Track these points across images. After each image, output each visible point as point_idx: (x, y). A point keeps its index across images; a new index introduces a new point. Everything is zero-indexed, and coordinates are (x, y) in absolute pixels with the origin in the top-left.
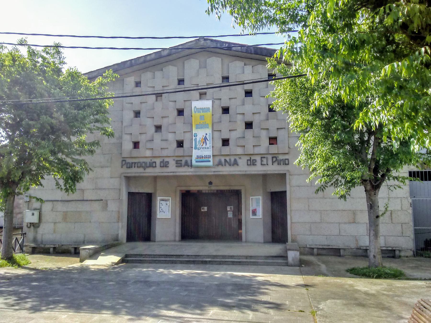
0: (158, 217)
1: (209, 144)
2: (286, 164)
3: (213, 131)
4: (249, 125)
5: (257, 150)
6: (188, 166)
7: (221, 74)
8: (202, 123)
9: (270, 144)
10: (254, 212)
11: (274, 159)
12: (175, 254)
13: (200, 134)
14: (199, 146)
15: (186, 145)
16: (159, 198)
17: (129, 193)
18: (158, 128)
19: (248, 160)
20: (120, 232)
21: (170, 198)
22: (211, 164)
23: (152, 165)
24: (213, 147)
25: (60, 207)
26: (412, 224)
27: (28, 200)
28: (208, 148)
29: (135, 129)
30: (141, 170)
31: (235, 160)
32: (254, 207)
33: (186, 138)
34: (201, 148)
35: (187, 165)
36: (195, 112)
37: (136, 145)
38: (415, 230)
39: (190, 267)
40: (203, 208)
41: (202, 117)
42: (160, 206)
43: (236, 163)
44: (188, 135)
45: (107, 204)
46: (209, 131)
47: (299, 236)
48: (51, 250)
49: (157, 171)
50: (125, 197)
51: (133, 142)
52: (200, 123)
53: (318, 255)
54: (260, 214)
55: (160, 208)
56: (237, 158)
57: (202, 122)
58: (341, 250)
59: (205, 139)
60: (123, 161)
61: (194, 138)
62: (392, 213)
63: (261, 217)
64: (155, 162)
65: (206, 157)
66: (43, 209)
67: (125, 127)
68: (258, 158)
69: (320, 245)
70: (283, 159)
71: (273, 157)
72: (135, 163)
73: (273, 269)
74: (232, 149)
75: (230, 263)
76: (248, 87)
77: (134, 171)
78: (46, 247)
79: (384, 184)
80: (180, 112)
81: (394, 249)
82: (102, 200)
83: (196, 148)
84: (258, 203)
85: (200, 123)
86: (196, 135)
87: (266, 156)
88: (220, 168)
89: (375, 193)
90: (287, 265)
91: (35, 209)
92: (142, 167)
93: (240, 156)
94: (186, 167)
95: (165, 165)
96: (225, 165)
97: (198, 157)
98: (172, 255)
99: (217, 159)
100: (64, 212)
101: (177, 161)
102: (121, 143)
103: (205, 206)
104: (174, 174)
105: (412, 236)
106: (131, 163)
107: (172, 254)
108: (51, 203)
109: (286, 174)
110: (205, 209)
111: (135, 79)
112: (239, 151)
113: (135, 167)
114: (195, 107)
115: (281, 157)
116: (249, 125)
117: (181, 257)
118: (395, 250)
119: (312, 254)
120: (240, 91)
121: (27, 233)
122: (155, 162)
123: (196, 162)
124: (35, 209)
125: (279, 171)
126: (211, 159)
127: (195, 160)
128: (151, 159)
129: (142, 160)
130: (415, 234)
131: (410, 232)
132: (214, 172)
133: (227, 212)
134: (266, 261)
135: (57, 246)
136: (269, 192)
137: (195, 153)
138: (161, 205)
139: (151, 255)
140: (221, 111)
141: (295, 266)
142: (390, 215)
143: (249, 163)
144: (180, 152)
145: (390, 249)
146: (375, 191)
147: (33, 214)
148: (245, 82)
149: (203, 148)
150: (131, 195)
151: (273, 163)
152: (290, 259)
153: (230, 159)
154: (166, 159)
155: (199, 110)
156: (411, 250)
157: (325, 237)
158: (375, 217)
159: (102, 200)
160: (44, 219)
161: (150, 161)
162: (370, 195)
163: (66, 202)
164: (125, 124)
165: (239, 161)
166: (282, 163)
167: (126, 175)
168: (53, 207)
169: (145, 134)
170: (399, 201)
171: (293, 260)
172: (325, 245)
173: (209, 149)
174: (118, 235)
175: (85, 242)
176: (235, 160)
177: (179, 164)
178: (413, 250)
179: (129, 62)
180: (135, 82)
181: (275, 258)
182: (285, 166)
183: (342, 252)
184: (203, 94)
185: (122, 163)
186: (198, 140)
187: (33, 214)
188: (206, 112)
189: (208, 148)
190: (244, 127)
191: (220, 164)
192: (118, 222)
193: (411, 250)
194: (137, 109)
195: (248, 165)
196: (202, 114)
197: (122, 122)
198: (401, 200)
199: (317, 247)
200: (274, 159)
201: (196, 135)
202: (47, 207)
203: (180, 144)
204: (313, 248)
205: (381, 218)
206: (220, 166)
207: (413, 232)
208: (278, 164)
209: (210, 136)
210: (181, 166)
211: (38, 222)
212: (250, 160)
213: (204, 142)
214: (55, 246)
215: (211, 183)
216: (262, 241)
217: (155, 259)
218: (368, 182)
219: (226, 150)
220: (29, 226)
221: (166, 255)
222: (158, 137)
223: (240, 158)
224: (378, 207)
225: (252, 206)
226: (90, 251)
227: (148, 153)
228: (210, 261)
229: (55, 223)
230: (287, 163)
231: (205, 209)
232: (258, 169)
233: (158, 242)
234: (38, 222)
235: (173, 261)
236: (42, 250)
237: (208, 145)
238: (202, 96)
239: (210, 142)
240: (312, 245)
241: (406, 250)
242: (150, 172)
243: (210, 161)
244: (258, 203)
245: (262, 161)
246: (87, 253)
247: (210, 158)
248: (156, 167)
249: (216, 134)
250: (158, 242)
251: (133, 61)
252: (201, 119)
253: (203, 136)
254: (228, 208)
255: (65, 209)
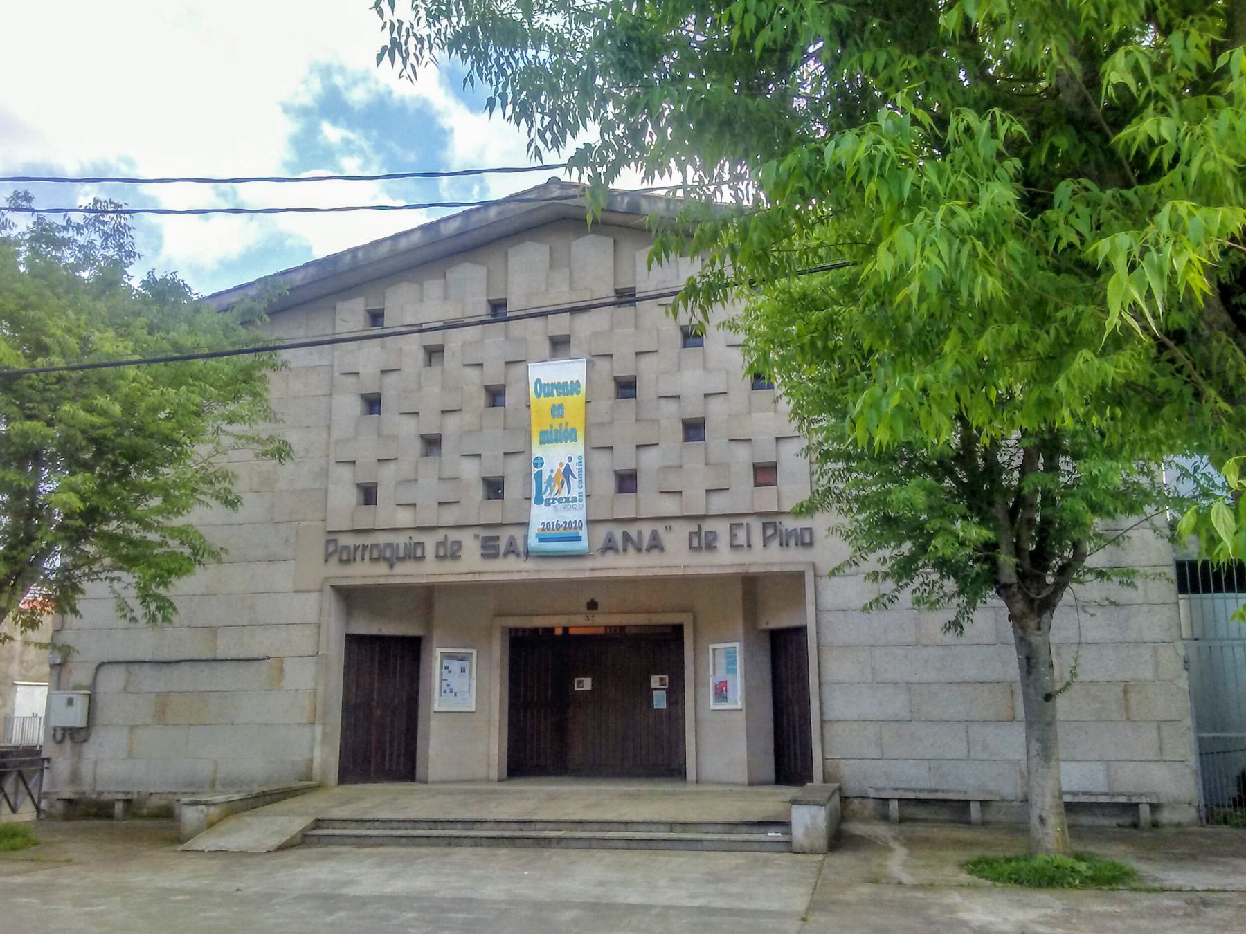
0: (436, 707)
1: (577, 488)
2: (803, 544)
3: (591, 448)
4: (694, 429)
5: (720, 504)
6: (518, 555)
7: (612, 283)
8: (556, 426)
9: (757, 485)
10: (721, 692)
11: (770, 532)
12: (459, 817)
13: (554, 457)
14: (551, 494)
15: (512, 490)
16: (438, 652)
17: (347, 636)
18: (432, 443)
19: (691, 533)
20: (318, 755)
21: (474, 652)
22: (583, 545)
23: (414, 554)
24: (587, 496)
25: (150, 680)
26: (1189, 722)
27: (58, 661)
28: (575, 500)
29: (366, 450)
30: (382, 568)
31: (655, 536)
32: (721, 675)
33: (513, 471)
34: (554, 499)
35: (513, 552)
36: (538, 395)
37: (369, 494)
38: (1201, 741)
39: (495, 855)
40: (579, 682)
41: (557, 411)
42: (441, 674)
43: (656, 545)
44: (516, 464)
45: (282, 670)
46: (576, 449)
47: (847, 762)
48: (119, 808)
49: (429, 571)
50: (336, 651)
51: (359, 485)
52: (551, 426)
53: (902, 820)
54: (736, 699)
55: (442, 680)
56: (660, 527)
57: (556, 423)
58: (972, 804)
59: (567, 472)
60: (329, 542)
61: (535, 470)
62: (1129, 689)
63: (739, 705)
64: (422, 545)
65: (569, 525)
66: (102, 688)
67: (337, 443)
68: (722, 528)
69: (906, 790)
70: (795, 530)
71: (765, 526)
72: (365, 547)
73: (741, 861)
74: (649, 501)
75: (620, 844)
76: (433, 339)
77: (365, 573)
78: (102, 798)
79: (1067, 596)
80: (495, 395)
81: (1135, 800)
82: (269, 658)
83: (539, 501)
84: (731, 662)
85: (551, 426)
86: (539, 462)
87: (745, 521)
88: (610, 560)
89: (1039, 623)
90: (788, 847)
91: (77, 688)
92: (386, 559)
93: (668, 523)
94: (512, 557)
95: (451, 552)
96: (625, 550)
97: (546, 527)
98: (452, 821)
99: (602, 532)
100: (158, 694)
101: (486, 539)
102: (326, 491)
103: (586, 676)
104: (477, 578)
105: (1193, 760)
106: (352, 547)
107: (452, 817)
108: (122, 668)
109: (804, 572)
110: (587, 684)
111: (367, 305)
112: (669, 506)
113: (363, 559)
114: (538, 381)
115: (789, 524)
116: (694, 429)
117: (478, 825)
118: (1137, 804)
119: (885, 818)
120: (413, 346)
121: (53, 759)
122: (422, 545)
123: (541, 540)
124: (77, 688)
125: (786, 564)
126: (583, 533)
127: (537, 535)
128: (411, 533)
129: (381, 539)
130: (1201, 754)
131: (1184, 749)
132: (593, 570)
133: (650, 691)
134: (726, 837)
135: (135, 797)
136: (764, 631)
137: (540, 516)
138: (445, 671)
139: (390, 821)
140: (611, 387)
141: (813, 852)
142: (1121, 695)
143: (695, 543)
144: (493, 512)
145: (1122, 799)
146: (1040, 616)
147: (70, 702)
148: (424, 326)
149: (560, 500)
150: (353, 641)
151: (766, 542)
152: (798, 832)
153: (640, 533)
154: (454, 536)
155: (546, 389)
156: (1190, 804)
157: (926, 763)
158: (1041, 699)
159: (269, 658)
160: (102, 717)
161: (406, 540)
162: (1023, 628)
163: (165, 666)
164: (336, 434)
165: (667, 539)
166: (792, 542)
167: (338, 583)
168: (127, 682)
169: (394, 462)
170: (1147, 653)
171: (807, 833)
172: (921, 790)
173: (578, 503)
174: (311, 760)
175: (217, 783)
176: (655, 536)
177: (490, 549)
178: (1196, 804)
179: (349, 257)
180: (369, 312)
181: (755, 829)
182: (800, 550)
183: (975, 812)
184: (437, 352)
185: (327, 549)
186: (545, 477)
187: (70, 702)
188: (570, 393)
189: (575, 500)
190: (680, 435)
191: (609, 547)
192: (313, 723)
193: (1190, 804)
194: (371, 389)
195: (691, 547)
196: (556, 399)
197: (329, 428)
198: (1156, 651)
199: (898, 795)
200: (770, 532)
201: (539, 462)
202: (111, 682)
203: (494, 488)
204: (887, 799)
205: (1061, 702)
206: (610, 554)
207: (1194, 746)
208: (781, 545)
209: (579, 464)
210: (495, 556)
211: (84, 725)
212: (698, 534)
213: (562, 484)
214: (129, 797)
215: (593, 605)
216: (746, 781)
217: (398, 833)
218: (1015, 589)
219: (626, 506)
220: (59, 737)
221: (435, 822)
222: (429, 468)
223: (668, 528)
224: (1051, 666)
225: (714, 674)
226: (212, 809)
227: (404, 518)
228: (560, 839)
229: (132, 728)
230: (807, 540)
231: (587, 684)
232: (723, 560)
233: (435, 782)
234: (84, 725)
235: (450, 837)
236: (94, 810)
237: (575, 493)
238: (559, 345)
239: (581, 481)
240: (884, 789)
241: (1175, 804)
242: (407, 573)
243: (579, 539)
244: (731, 662)
245: (733, 536)
246: (202, 816)
247: (581, 528)
248: (423, 557)
249: (602, 460)
250: (435, 782)
251: (360, 254)
252: (553, 416)
253: (561, 464)
254: (655, 681)
255: (161, 687)
